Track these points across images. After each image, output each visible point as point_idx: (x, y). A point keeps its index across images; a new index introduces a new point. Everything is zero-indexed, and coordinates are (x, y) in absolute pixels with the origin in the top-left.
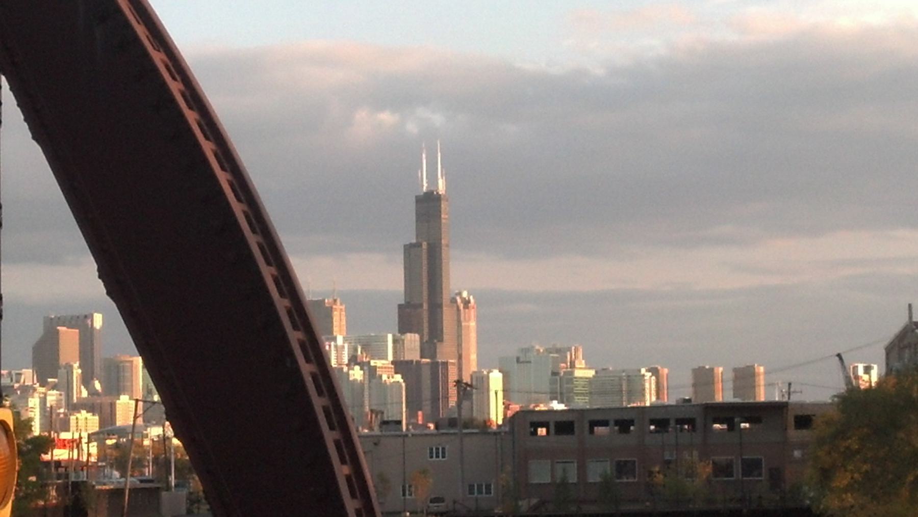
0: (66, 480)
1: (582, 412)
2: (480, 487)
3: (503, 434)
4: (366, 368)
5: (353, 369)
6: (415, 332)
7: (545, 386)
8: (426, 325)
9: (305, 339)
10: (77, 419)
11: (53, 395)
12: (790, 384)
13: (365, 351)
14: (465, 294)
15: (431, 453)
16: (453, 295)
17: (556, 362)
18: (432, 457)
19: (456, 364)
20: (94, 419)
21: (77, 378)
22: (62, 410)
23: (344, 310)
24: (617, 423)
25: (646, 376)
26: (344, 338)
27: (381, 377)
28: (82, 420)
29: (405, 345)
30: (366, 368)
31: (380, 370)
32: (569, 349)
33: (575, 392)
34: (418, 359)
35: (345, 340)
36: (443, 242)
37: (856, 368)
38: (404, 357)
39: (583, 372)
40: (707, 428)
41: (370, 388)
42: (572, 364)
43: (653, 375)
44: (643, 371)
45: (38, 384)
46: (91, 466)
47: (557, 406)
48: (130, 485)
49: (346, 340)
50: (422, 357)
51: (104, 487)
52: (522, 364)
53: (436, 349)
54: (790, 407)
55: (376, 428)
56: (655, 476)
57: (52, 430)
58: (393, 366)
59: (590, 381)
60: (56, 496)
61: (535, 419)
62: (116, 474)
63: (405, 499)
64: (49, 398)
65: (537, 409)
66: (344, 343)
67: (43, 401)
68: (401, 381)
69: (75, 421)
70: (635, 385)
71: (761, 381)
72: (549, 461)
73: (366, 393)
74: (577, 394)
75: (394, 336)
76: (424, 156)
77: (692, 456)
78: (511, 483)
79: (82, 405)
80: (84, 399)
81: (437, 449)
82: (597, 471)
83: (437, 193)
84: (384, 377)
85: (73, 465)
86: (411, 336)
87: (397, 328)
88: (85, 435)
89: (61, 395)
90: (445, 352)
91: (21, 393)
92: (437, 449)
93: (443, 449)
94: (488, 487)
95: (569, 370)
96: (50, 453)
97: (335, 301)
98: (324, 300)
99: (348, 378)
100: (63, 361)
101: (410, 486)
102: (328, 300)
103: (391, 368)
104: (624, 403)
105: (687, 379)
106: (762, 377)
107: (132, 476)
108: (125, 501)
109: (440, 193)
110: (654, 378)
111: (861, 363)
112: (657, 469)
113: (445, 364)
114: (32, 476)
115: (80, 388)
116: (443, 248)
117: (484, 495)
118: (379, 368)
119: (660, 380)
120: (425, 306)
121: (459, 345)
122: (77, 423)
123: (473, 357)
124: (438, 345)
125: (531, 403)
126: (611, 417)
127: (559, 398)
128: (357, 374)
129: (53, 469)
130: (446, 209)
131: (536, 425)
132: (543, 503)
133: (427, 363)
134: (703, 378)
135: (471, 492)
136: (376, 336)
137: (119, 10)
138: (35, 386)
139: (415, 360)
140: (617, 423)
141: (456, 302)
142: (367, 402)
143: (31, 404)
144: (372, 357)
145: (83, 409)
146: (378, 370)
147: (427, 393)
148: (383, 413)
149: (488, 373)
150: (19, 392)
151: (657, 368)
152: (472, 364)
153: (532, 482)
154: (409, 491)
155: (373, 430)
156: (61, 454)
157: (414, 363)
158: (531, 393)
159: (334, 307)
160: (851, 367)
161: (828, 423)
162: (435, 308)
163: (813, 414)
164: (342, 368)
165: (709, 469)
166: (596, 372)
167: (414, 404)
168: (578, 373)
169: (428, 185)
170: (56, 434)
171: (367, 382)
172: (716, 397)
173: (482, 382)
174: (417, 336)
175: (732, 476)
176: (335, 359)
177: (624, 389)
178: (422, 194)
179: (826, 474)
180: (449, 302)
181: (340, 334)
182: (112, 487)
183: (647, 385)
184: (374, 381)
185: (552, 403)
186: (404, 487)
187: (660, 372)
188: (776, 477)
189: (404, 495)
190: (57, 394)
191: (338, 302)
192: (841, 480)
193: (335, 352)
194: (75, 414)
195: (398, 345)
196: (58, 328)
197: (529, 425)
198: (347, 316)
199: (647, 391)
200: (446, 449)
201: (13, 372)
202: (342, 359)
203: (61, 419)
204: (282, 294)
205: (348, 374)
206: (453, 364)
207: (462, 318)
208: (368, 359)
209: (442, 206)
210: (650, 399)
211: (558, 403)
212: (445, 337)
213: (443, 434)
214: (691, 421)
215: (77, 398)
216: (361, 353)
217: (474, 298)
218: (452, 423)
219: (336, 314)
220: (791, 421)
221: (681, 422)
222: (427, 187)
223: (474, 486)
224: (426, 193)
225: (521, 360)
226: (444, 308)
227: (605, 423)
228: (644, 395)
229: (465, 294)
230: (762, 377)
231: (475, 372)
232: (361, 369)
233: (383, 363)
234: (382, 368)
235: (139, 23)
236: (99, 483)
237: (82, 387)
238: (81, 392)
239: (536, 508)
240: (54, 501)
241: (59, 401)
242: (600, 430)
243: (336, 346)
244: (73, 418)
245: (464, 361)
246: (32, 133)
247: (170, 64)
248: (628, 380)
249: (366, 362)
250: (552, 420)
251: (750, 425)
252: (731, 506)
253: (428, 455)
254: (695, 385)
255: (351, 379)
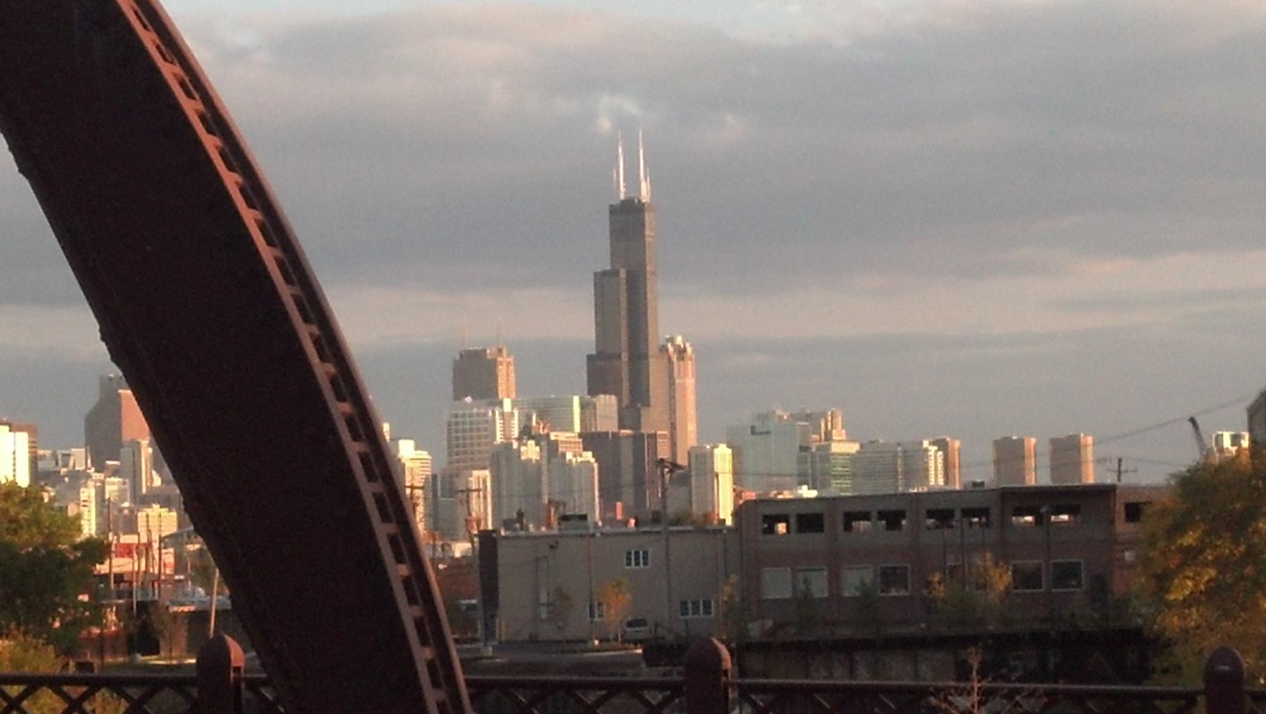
0: (130, 600)
1: (834, 500)
2: (695, 604)
3: (725, 532)
4: (543, 443)
5: (526, 445)
6: (610, 394)
7: (791, 466)
8: (626, 385)
9: (354, 412)
10: (147, 516)
11: (114, 483)
12: (1120, 460)
13: (542, 419)
14: (679, 340)
15: (629, 559)
16: (662, 342)
17: (805, 433)
18: (629, 564)
19: (669, 435)
20: (170, 516)
21: (146, 460)
22: (126, 504)
23: (512, 363)
24: (882, 515)
25: (931, 451)
26: (512, 401)
27: (564, 455)
28: (153, 517)
29: (598, 412)
30: (543, 443)
31: (564, 445)
32: (824, 415)
33: (833, 473)
34: (616, 430)
35: (514, 405)
36: (648, 268)
37: (1220, 438)
38: (596, 428)
39: (842, 447)
40: (1004, 524)
41: (549, 470)
42: (828, 435)
43: (939, 450)
44: (926, 444)
45: (93, 469)
46: (164, 581)
47: (807, 493)
48: (217, 605)
49: (516, 405)
50: (621, 426)
51: (181, 609)
52: (759, 437)
53: (639, 416)
54: (1117, 492)
55: (555, 524)
56: (935, 589)
57: (110, 531)
58: (580, 440)
59: (854, 458)
60: (117, 621)
61: (768, 511)
62: (201, 591)
63: (592, 622)
64: (108, 488)
65: (780, 497)
66: (513, 408)
67: (101, 492)
68: (593, 460)
69: (145, 519)
70: (914, 463)
71: (1089, 454)
72: (789, 569)
73: (544, 479)
74: (835, 477)
75: (581, 399)
76: (620, 149)
77: (985, 561)
78: (737, 599)
79: (154, 496)
80: (157, 488)
81: (637, 553)
82: (855, 580)
83: (639, 201)
84: (569, 456)
85: (141, 579)
86: (605, 399)
87: (586, 387)
88: (155, 537)
89: (124, 483)
90: (653, 420)
91: (70, 480)
92: (637, 553)
93: (645, 553)
94: (707, 606)
95: (823, 443)
96: (107, 562)
97: (500, 351)
98: (485, 350)
99: (519, 457)
100: (127, 436)
101: (600, 604)
102: (491, 350)
103: (579, 443)
104: (900, 489)
105: (988, 453)
106: (1090, 449)
107: (218, 594)
108: (209, 629)
109: (644, 201)
110: (940, 453)
111: (1227, 431)
112: (936, 579)
113: (653, 437)
114: (83, 593)
115: (151, 473)
116: (648, 276)
117: (690, 616)
118: (562, 442)
119: (950, 454)
120: (625, 357)
121: (672, 411)
122: (148, 521)
123: (692, 427)
124: (644, 412)
125: (771, 490)
126: (874, 509)
127: (810, 482)
128: (531, 451)
129: (113, 586)
130: (651, 222)
131: (772, 520)
132: (780, 626)
133: (628, 436)
134: (1009, 452)
135: (684, 611)
136: (557, 399)
137: (120, 14)
138: (88, 471)
139: (610, 432)
140: (882, 515)
141: (667, 350)
142: (545, 490)
143: (83, 496)
144: (553, 428)
145: (154, 503)
146: (560, 445)
147: (627, 476)
148: (565, 505)
149: (712, 448)
150: (67, 479)
151: (944, 440)
152: (690, 435)
153: (764, 597)
154: (599, 610)
155: (552, 528)
156: (121, 564)
157: (610, 436)
158: (770, 475)
159: (499, 359)
160: (1214, 436)
161: (1163, 513)
162: (638, 357)
163: (1144, 500)
164: (511, 444)
165: (1008, 578)
166: (862, 446)
167: (610, 493)
168: (836, 448)
169: (627, 189)
170: (115, 537)
171: (545, 462)
172: (1027, 478)
173: (703, 460)
174: (613, 399)
175: (1040, 587)
176: (501, 431)
177: (900, 470)
178: (618, 202)
179: (1163, 580)
180: (657, 350)
181: (508, 397)
182: (192, 608)
183: (932, 464)
184: (555, 460)
185: (801, 489)
186: (591, 607)
187: (950, 444)
188: (1100, 586)
189: (592, 615)
190: (119, 482)
191: (505, 352)
192: (1182, 589)
193: (502, 421)
194: (144, 509)
195: (588, 411)
196: (120, 391)
197: (760, 519)
198: (516, 371)
199: (932, 472)
200: (650, 554)
201: (60, 453)
202: (510, 431)
203: (125, 517)
204: (323, 358)
205: (519, 451)
206: (663, 436)
207: (676, 375)
208: (546, 431)
209: (647, 218)
210: (936, 480)
211: (809, 489)
212: (652, 401)
213: (644, 533)
214: (982, 512)
215: (147, 487)
216: (538, 423)
217: (691, 346)
218: (656, 518)
219: (502, 370)
220: (1120, 510)
221: (968, 513)
222: (626, 193)
223: (699, 602)
224: (622, 202)
225: (757, 430)
226: (651, 360)
227: (865, 516)
228: (927, 477)
229: (679, 340)
230: (1090, 449)
231: (692, 448)
232: (537, 444)
233: (567, 436)
234: (566, 442)
235: (145, 27)
236: (174, 603)
237: (154, 473)
238: (152, 479)
239: (772, 632)
240: (113, 628)
241: (122, 493)
242: (863, 525)
243: (502, 414)
244: (141, 516)
245: (679, 434)
246: (19, 165)
247: (187, 80)
248: (905, 457)
249: (543, 435)
250: (793, 511)
251: (1069, 518)
252: (1037, 626)
253: (625, 561)
254: (997, 462)
255: (523, 458)
